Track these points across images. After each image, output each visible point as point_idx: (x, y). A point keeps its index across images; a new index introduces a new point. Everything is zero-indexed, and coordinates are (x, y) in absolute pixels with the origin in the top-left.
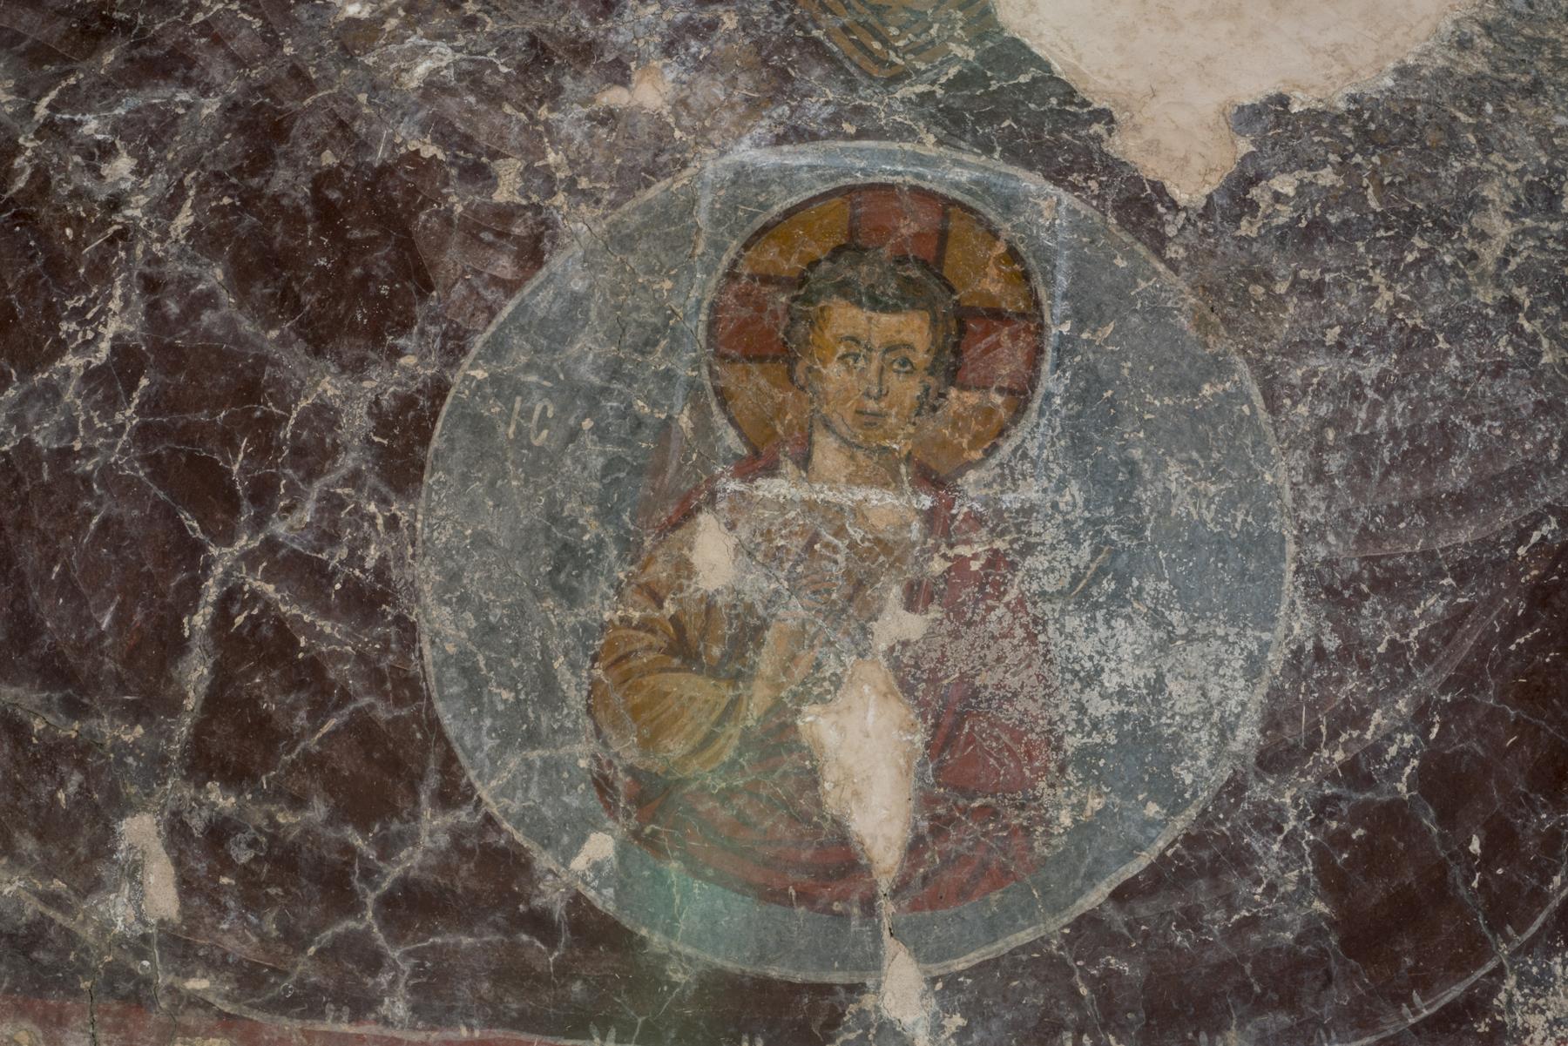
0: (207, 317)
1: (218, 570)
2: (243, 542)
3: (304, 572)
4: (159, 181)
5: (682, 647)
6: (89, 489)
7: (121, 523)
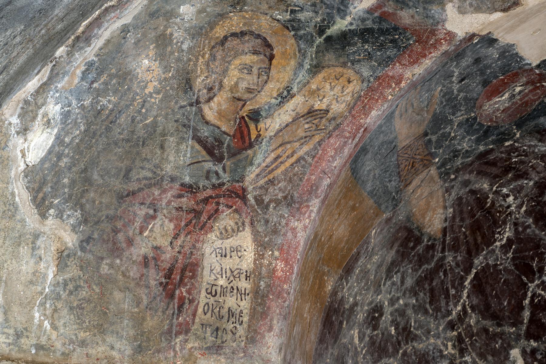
0: (528, 230)
1: (531, 289)
2: (536, 282)
4: (519, 201)
6: (501, 273)
7: (508, 280)
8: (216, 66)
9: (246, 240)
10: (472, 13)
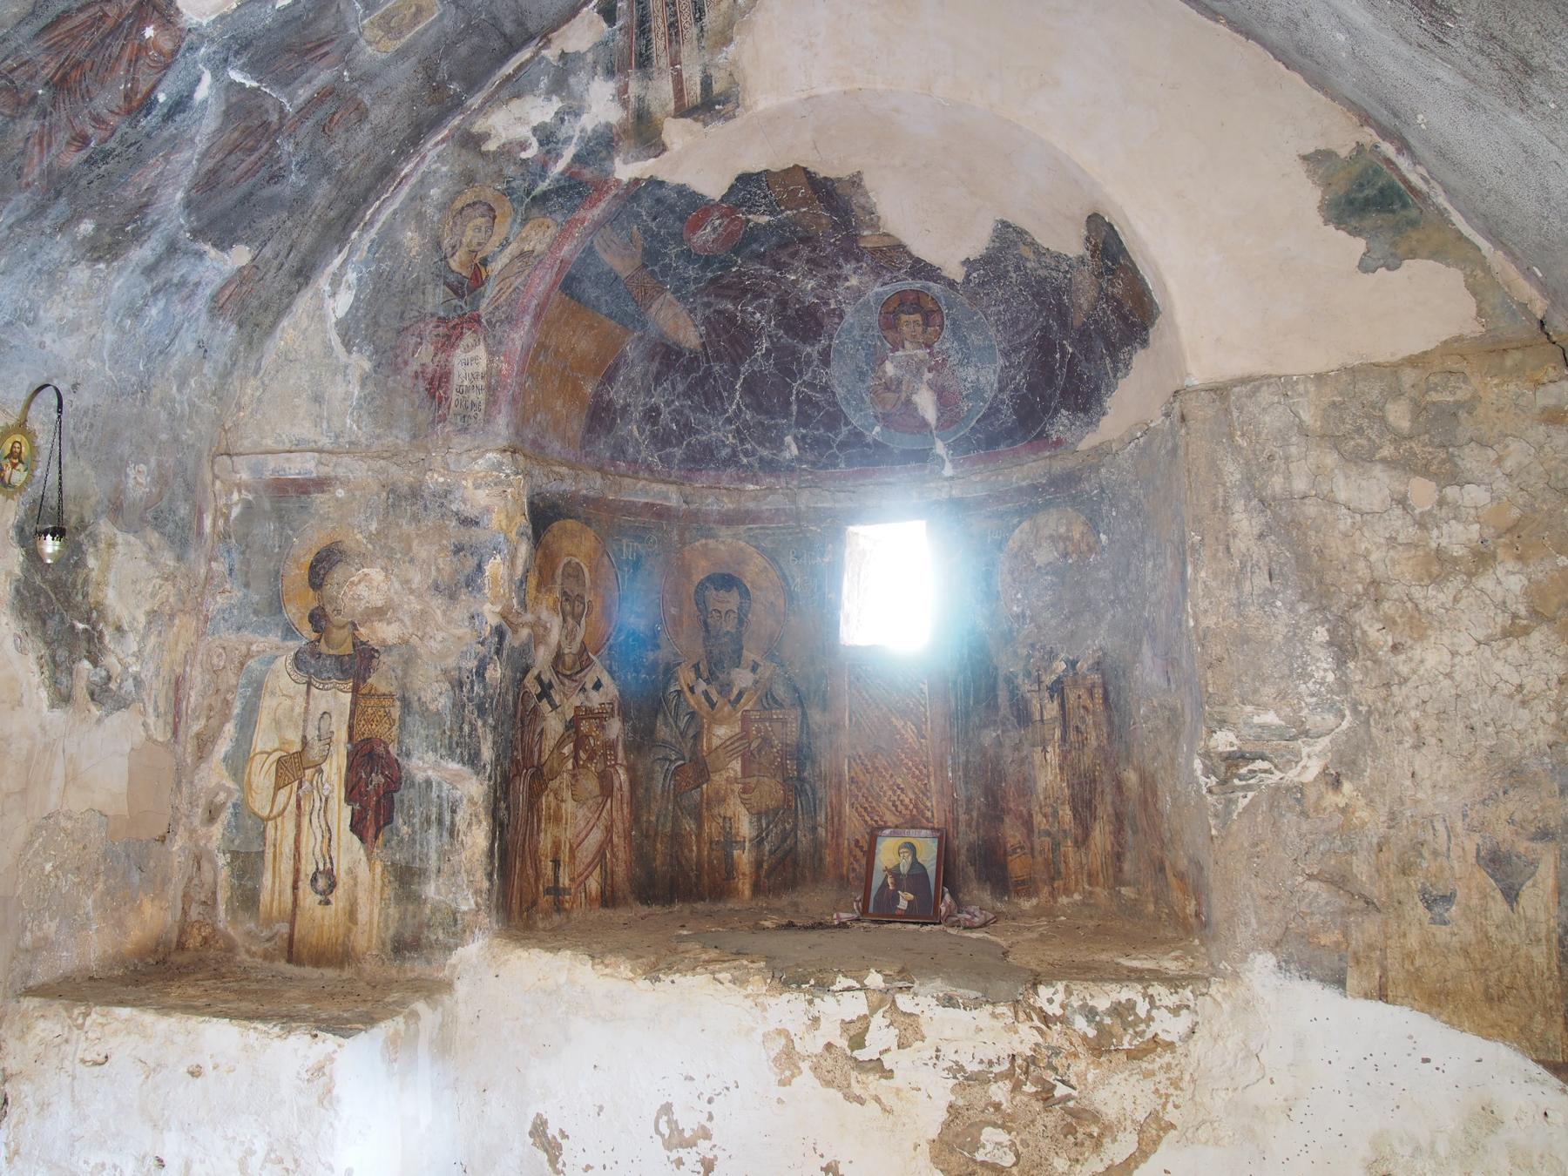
3: (811, 385)
5: (887, 388)
8: (458, 230)
9: (481, 352)
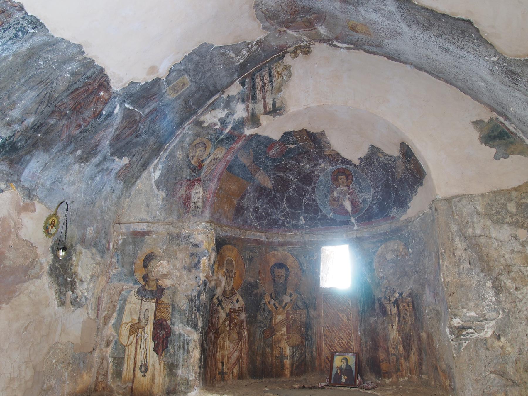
5: (334, 200)
8: (194, 151)
9: (201, 190)
10: (317, 133)
